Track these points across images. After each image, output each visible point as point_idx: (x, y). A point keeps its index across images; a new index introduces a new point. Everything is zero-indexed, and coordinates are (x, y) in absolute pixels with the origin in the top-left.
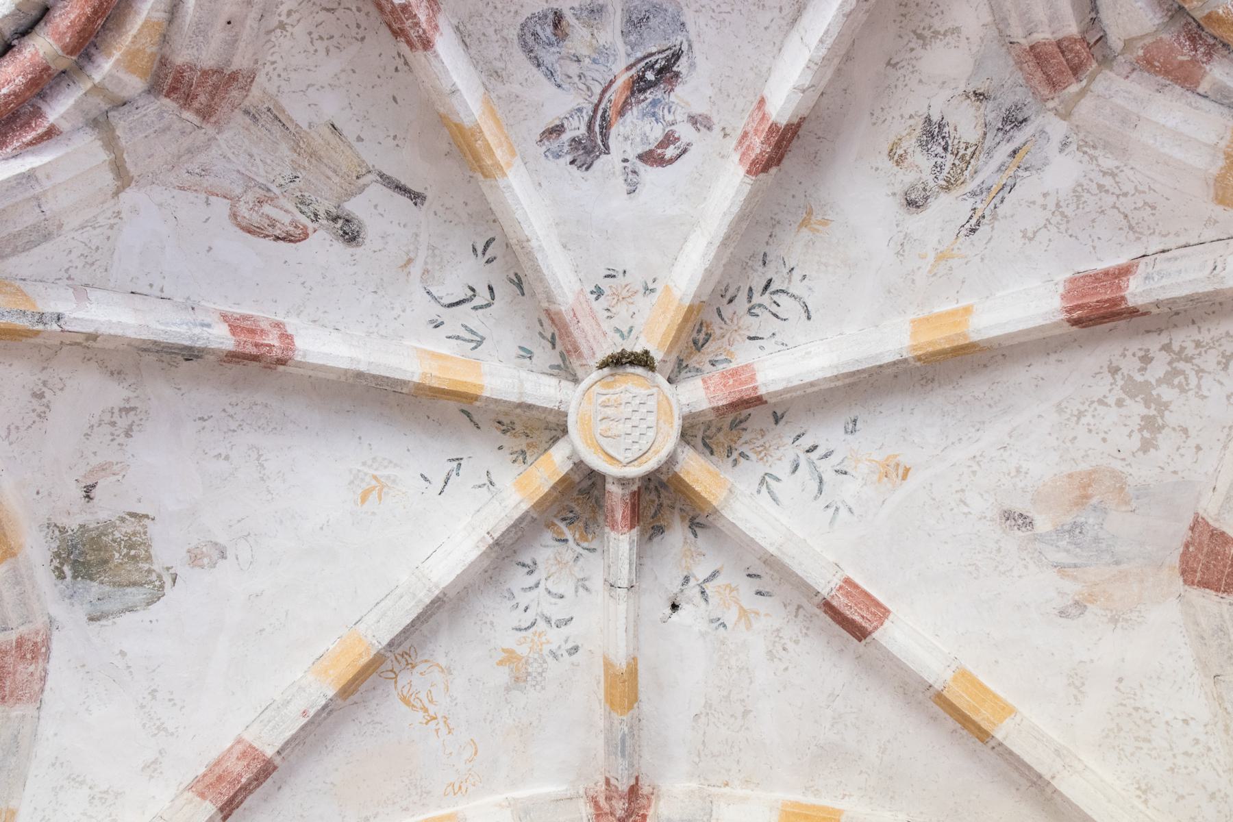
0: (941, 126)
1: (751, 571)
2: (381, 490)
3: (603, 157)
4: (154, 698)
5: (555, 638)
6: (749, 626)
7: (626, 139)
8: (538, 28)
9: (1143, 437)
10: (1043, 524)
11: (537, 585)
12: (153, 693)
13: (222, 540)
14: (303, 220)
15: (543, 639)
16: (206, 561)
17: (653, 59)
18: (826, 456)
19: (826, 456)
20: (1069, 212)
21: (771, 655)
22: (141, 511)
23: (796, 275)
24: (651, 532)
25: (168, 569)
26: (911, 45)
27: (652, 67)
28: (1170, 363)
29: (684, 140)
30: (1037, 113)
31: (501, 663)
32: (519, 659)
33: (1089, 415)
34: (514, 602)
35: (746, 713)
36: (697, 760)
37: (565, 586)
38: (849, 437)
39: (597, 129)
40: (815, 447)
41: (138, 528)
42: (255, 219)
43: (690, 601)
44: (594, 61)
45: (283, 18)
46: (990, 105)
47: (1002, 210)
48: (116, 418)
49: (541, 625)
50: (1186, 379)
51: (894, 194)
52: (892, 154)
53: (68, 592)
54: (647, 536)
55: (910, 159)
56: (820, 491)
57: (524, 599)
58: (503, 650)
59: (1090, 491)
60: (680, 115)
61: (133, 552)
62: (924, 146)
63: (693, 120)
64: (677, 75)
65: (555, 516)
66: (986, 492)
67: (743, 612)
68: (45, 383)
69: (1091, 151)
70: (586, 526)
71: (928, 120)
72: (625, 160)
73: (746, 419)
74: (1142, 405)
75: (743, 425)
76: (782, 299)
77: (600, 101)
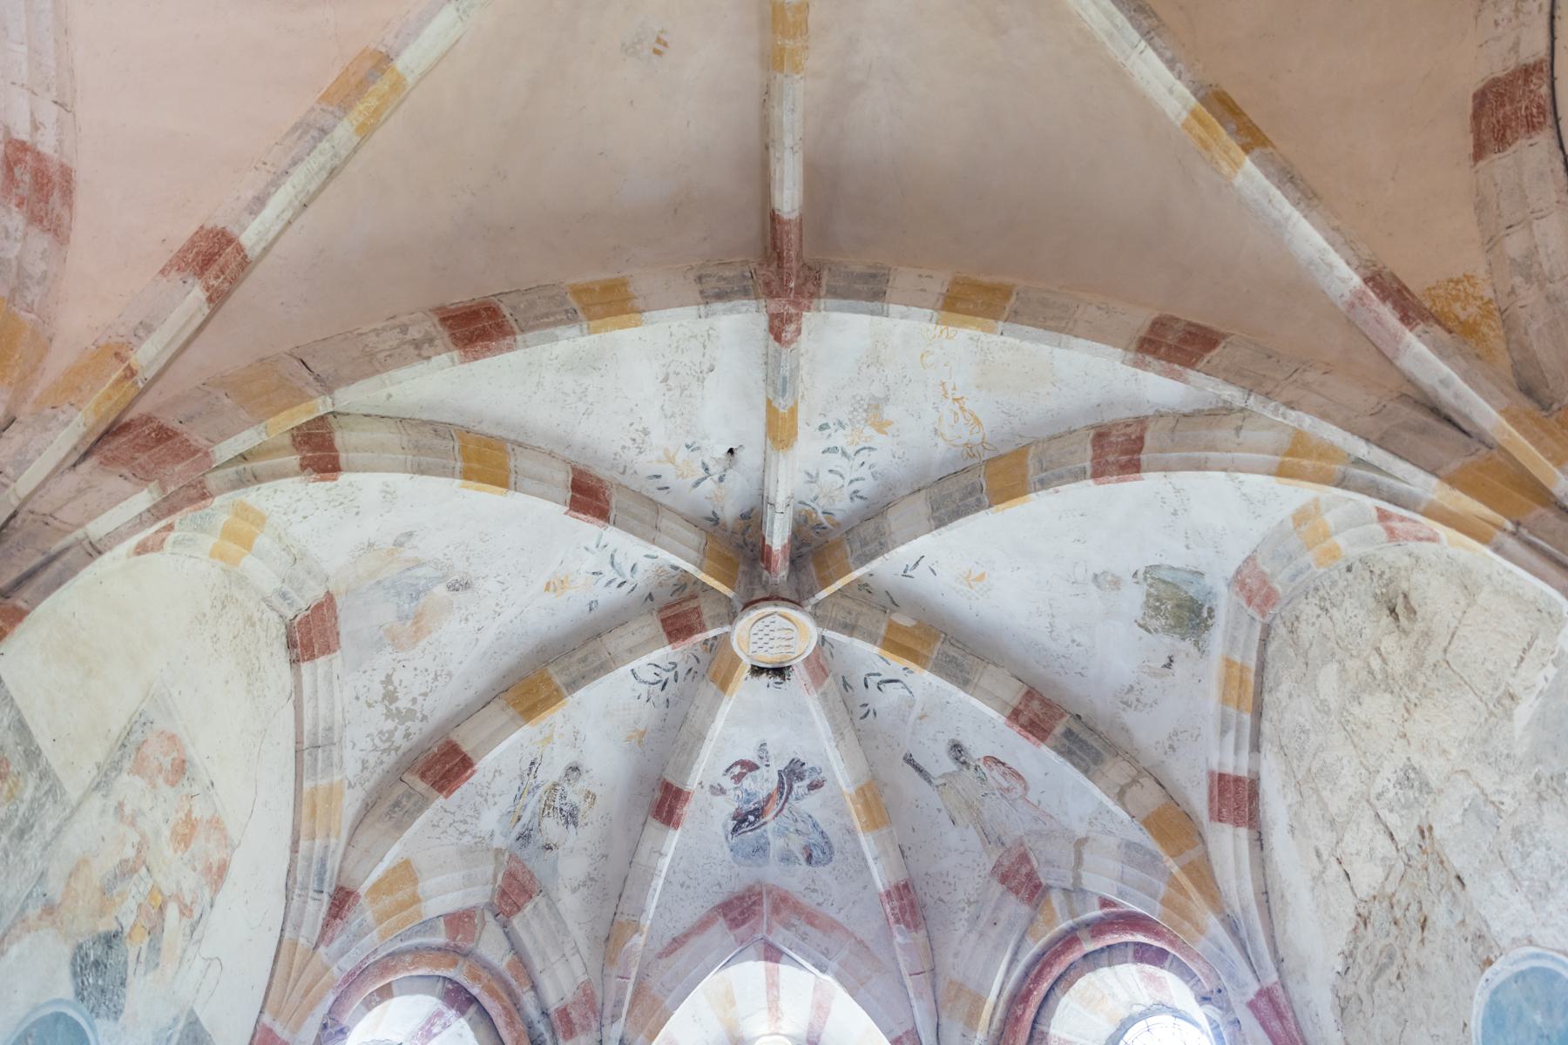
1: (666, 491)
2: (968, 577)
3: (782, 768)
4: (1175, 511)
5: (839, 439)
6: (666, 451)
7: (767, 780)
8: (821, 856)
9: (392, 684)
10: (440, 590)
11: (851, 482)
12: (1175, 513)
13: (1092, 588)
14: (985, 769)
15: (850, 439)
16: (1109, 578)
17: (750, 828)
18: (610, 582)
19: (610, 582)
20: (479, 799)
21: (646, 432)
23: (644, 697)
24: (752, 515)
25: (1137, 583)
26: (596, 873)
27: (750, 823)
28: (393, 742)
29: (728, 777)
30: (511, 846)
31: (890, 423)
32: (873, 425)
33: (430, 681)
34: (873, 470)
35: (666, 379)
36: (711, 332)
37: (826, 479)
38: (593, 599)
39: (786, 786)
40: (619, 586)
41: (1148, 620)
42: (1014, 782)
43: (718, 461)
44: (787, 829)
45: (967, 909)
46: (541, 843)
49: (851, 450)
50: (381, 740)
51: (587, 772)
52: (593, 797)
53: (1210, 596)
54: (755, 512)
55: (582, 797)
56: (612, 556)
57: (864, 472)
58: (886, 434)
59: (414, 629)
60: (731, 794)
61: (1158, 604)
62: (575, 808)
63: (722, 791)
64: (734, 819)
65: (831, 531)
66: (485, 596)
67: (671, 460)
68: (1166, 753)
69: (477, 840)
70: (806, 521)
71: (575, 824)
72: (767, 766)
73: (674, 592)
74: (401, 708)
75: (676, 587)
76: (653, 678)
77: (784, 804)
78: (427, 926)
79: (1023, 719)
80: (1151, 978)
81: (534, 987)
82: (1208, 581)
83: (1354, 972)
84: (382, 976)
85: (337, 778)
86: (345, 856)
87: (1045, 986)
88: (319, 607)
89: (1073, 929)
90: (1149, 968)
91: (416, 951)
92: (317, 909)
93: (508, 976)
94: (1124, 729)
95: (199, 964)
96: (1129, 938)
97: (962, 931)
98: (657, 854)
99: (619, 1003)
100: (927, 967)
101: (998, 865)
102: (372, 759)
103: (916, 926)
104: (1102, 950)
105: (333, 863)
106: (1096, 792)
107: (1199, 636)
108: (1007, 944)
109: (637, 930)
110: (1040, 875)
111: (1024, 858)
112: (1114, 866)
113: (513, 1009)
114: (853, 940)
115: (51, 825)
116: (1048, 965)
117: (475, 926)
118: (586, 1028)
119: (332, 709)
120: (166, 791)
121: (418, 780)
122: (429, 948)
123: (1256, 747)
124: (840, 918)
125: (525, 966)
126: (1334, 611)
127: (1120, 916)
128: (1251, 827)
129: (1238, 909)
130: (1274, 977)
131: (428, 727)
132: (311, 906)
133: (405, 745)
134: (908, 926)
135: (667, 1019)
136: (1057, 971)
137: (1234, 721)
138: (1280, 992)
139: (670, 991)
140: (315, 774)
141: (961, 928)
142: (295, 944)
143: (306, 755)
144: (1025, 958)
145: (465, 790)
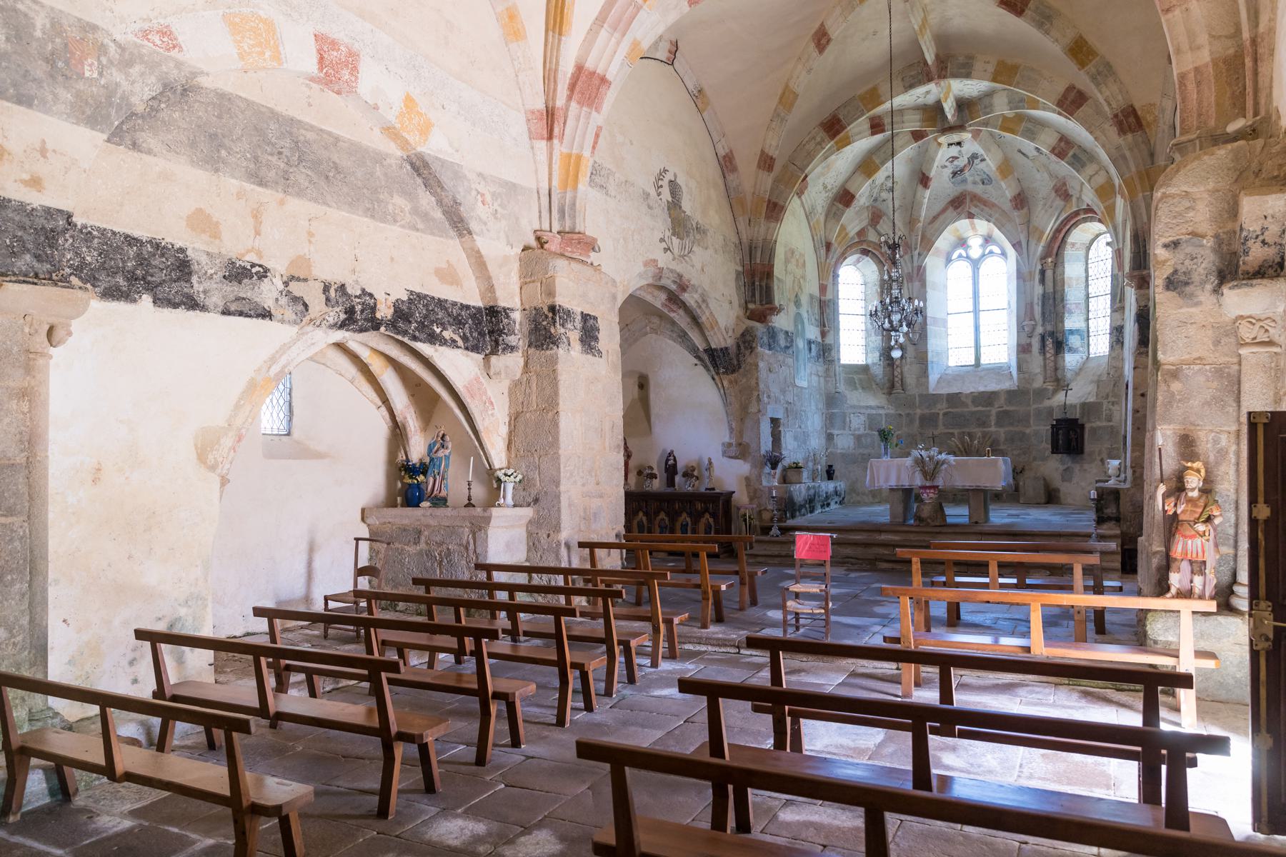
63: (946, 167)
78: (853, 238)
79: (1056, 151)
87: (1068, 227)
92: (823, 251)
97: (1039, 209)
99: (916, 244)
100: (1026, 220)
101: (1055, 185)
103: (1022, 208)
109: (919, 222)
111: (1064, 184)
116: (1069, 221)
124: (996, 202)
141: (1040, 208)
144: (1061, 219)
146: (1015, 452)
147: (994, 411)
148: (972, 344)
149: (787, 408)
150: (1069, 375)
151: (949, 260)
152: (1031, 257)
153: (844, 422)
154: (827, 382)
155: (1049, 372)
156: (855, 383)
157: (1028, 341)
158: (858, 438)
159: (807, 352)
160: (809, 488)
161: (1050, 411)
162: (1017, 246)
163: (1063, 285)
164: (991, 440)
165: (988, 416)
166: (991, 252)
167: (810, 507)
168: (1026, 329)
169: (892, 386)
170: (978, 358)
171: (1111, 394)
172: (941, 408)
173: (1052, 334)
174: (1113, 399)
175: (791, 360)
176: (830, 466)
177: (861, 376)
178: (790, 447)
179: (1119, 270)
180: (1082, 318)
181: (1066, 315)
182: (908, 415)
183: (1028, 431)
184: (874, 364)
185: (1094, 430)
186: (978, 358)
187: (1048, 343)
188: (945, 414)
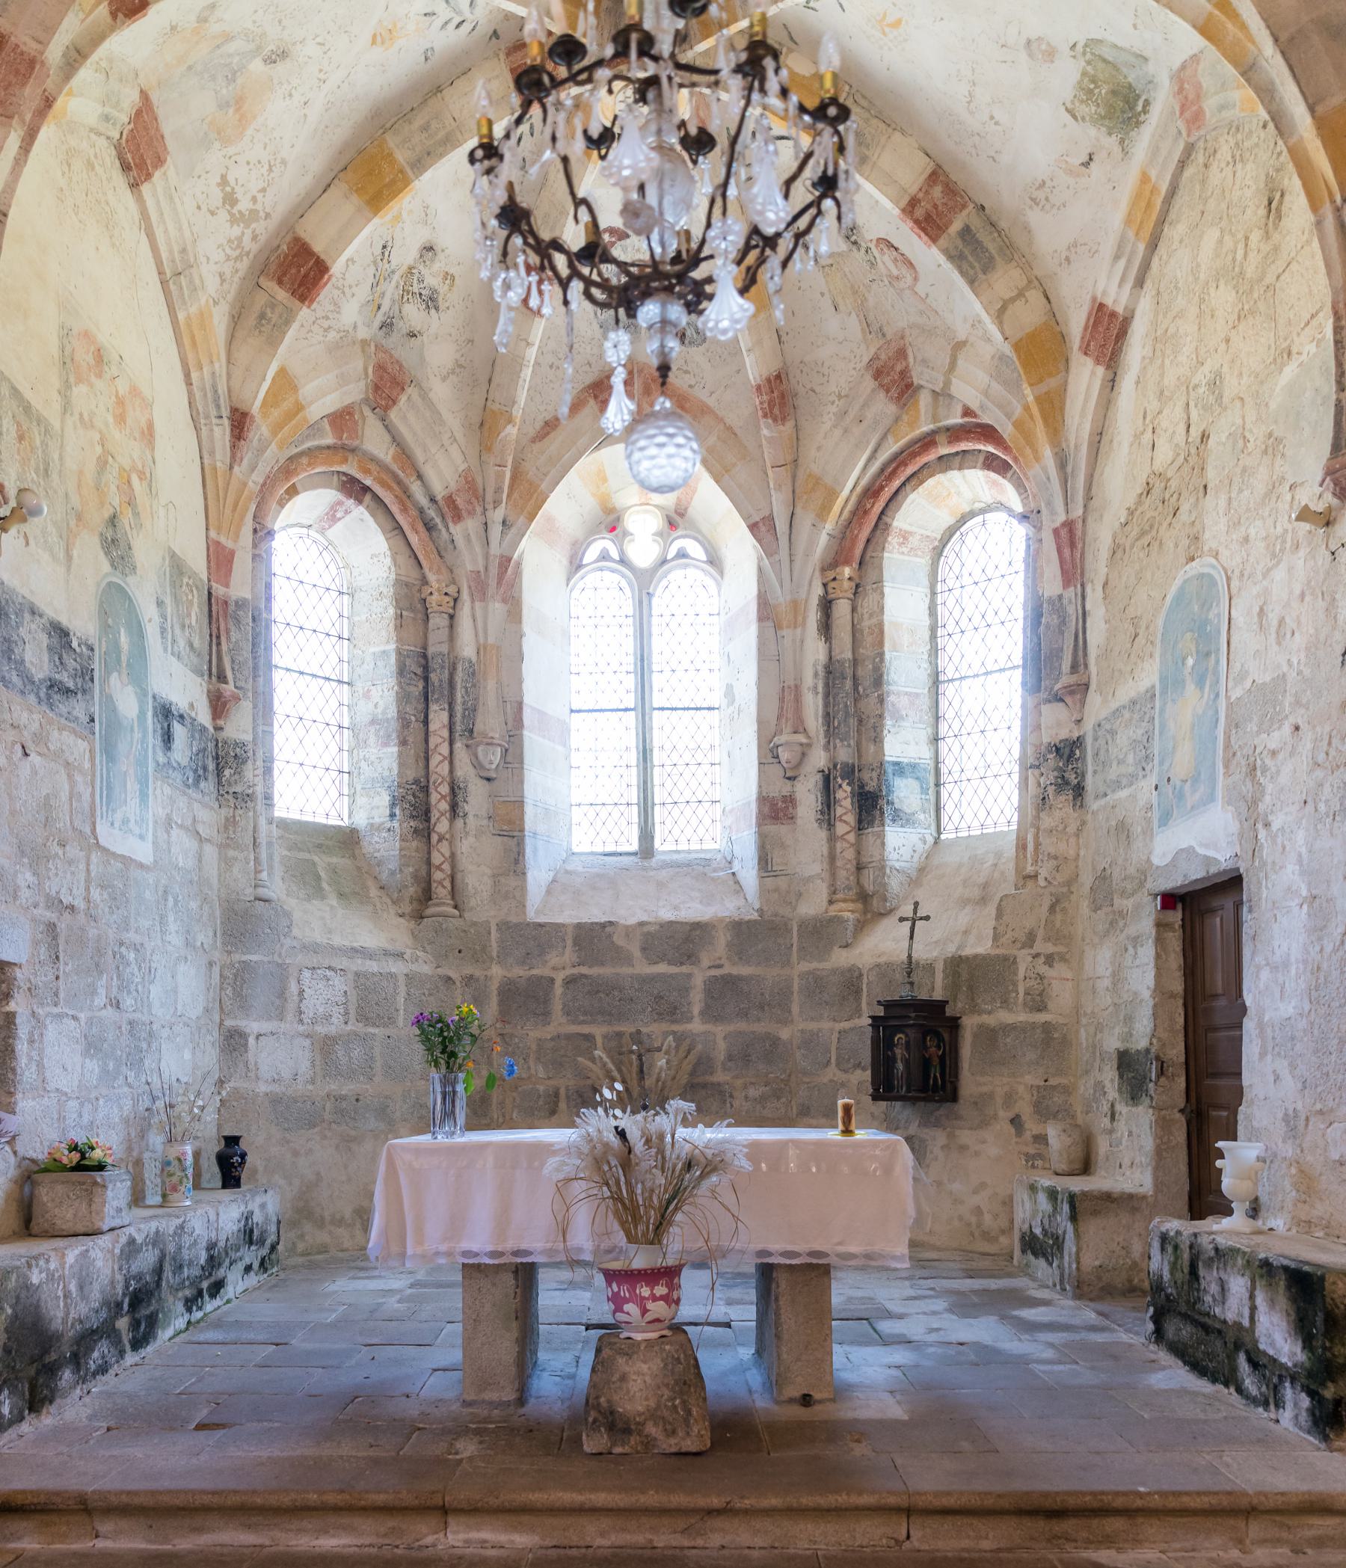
0: (428, 307)
10: (257, 66)
13: (1023, 56)
16: (1043, 47)
22: (1068, 116)
25: (1074, 57)
38: (429, 46)
40: (457, 27)
42: (904, 270)
46: (405, 331)
47: (372, 270)
48: (1043, 202)
53: (1150, 86)
55: (440, 279)
59: (237, 116)
62: (434, 291)
71: (437, 309)
78: (314, 428)
79: (919, 213)
80: (995, 483)
81: (420, 477)
82: (1151, 68)
83: (1128, 528)
84: (287, 479)
85: (203, 301)
86: (229, 376)
87: (897, 483)
88: (139, 113)
89: (934, 433)
90: (993, 475)
91: (309, 452)
92: (222, 433)
93: (395, 467)
94: (1027, 229)
95: (162, 512)
96: (981, 447)
98: (524, 343)
99: (498, 490)
100: (789, 458)
101: (875, 358)
102: (227, 270)
103: (784, 419)
104: (957, 453)
105: (222, 389)
106: (978, 307)
107: (1127, 133)
108: (868, 443)
109: (510, 420)
110: (913, 374)
111: (902, 353)
112: (982, 378)
113: (404, 498)
114: (721, 426)
115: (56, 456)
116: (904, 464)
117: (356, 423)
118: (471, 513)
119: (180, 229)
120: (99, 384)
121: (277, 288)
122: (320, 448)
123: (1140, 283)
124: (711, 402)
125: (408, 457)
126: (1239, 166)
127: (979, 425)
128: (1108, 367)
129: (1072, 446)
130: (1080, 512)
131: (272, 224)
132: (217, 431)
133: (255, 248)
134: (775, 420)
135: (544, 501)
136: (910, 470)
137: (1128, 249)
138: (1079, 525)
139: (545, 475)
140: (184, 303)
141: (828, 421)
142: (215, 469)
143: (172, 287)
144: (884, 456)
145: (326, 294)
146: (753, 1092)
147: (699, 980)
148: (633, 795)
149: (51, 927)
150: (894, 884)
151: (575, 565)
152: (797, 565)
153: (282, 994)
154: (226, 862)
155: (842, 874)
156: (318, 878)
157: (786, 788)
158: (326, 1046)
159: (154, 741)
160: (132, 1248)
161: (851, 982)
162: (761, 528)
163: (881, 643)
164: (692, 1057)
165: (684, 991)
166: (682, 554)
167: (135, 1325)
168: (784, 755)
169: (426, 895)
170: (646, 835)
171: (1040, 934)
172: (559, 964)
173: (850, 772)
174: (1050, 948)
175: (82, 745)
176: (232, 1141)
177: (334, 860)
178: (59, 1080)
179: (1067, 581)
180: (924, 734)
181: (888, 722)
182: (469, 980)
183: (785, 1034)
184: (373, 827)
185: (990, 1036)
186: (646, 835)
187: (840, 795)
188: (570, 982)
